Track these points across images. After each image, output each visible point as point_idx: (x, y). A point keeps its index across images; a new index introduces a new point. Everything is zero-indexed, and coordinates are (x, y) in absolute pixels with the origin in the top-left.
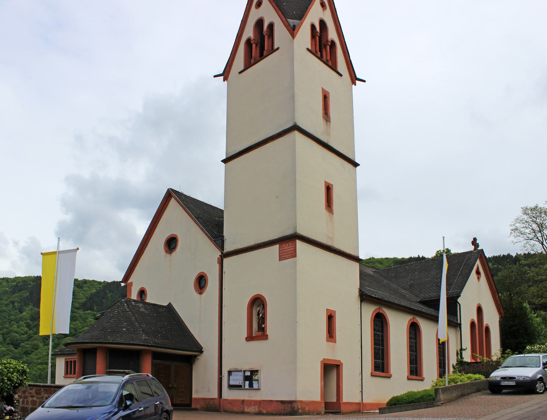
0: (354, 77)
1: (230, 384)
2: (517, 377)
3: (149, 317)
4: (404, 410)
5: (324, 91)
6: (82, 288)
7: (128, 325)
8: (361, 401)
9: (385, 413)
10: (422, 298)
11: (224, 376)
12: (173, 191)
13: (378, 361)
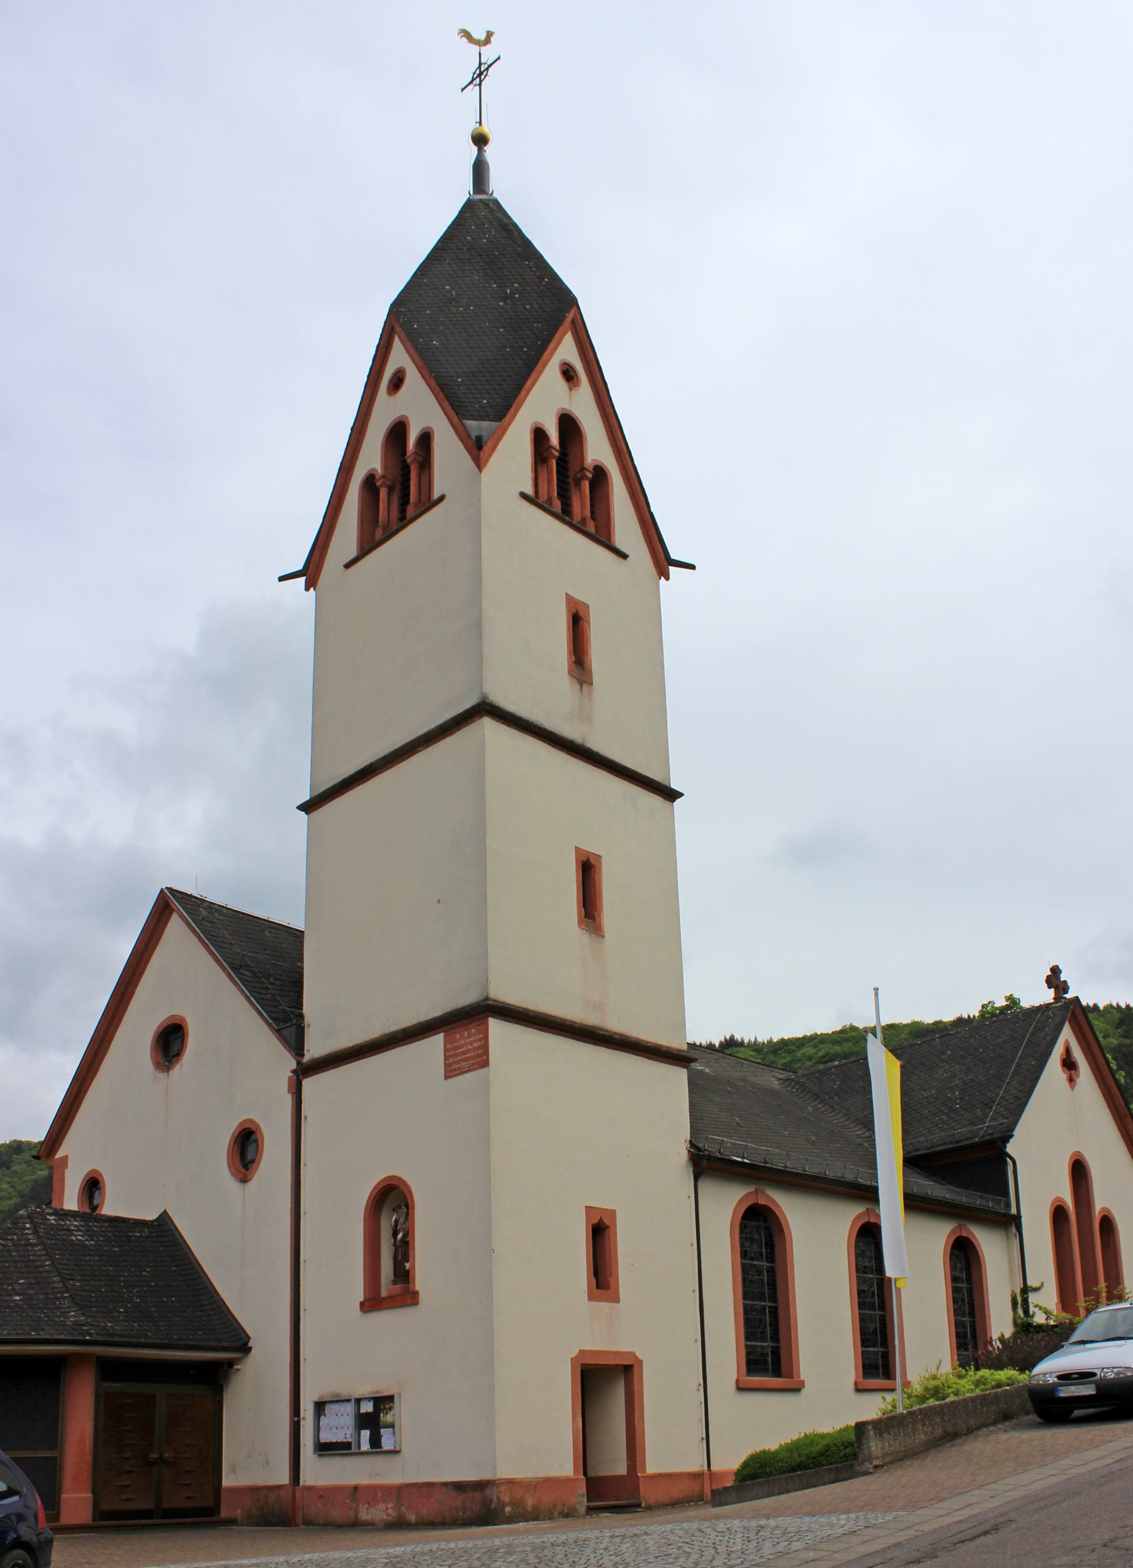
0: (663, 558)
1: (322, 1440)
2: (1098, 1372)
3: (97, 1258)
4: (777, 1492)
5: (570, 600)
6: (8, 1168)
7: (30, 1284)
9: (727, 1504)
10: (909, 1150)
11: (304, 1418)
12: (174, 896)
13: (758, 1344)
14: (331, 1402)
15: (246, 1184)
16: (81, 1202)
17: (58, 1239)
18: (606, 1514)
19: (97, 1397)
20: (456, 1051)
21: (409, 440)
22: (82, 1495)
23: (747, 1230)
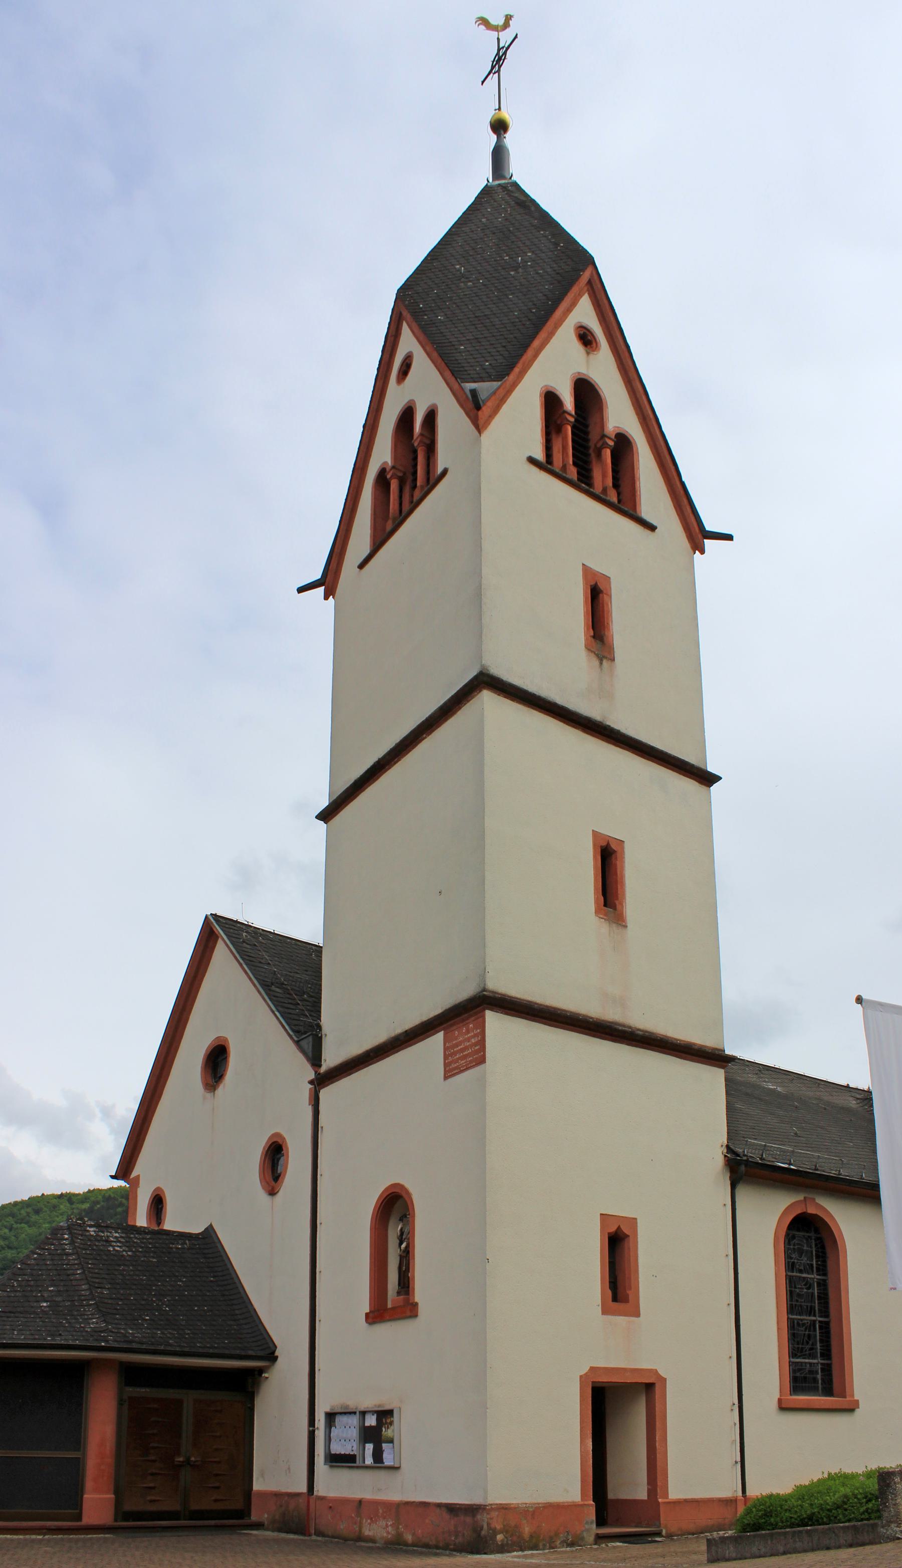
5: (586, 570)
8: (740, 1493)
11: (318, 1428)
13: (807, 1361)
14: (341, 1413)
15: (274, 1197)
16: (149, 1219)
17: (94, 1250)
18: (618, 1544)
19: (121, 1402)
20: (455, 1049)
21: (416, 423)
22: (102, 1496)
23: (795, 1241)
